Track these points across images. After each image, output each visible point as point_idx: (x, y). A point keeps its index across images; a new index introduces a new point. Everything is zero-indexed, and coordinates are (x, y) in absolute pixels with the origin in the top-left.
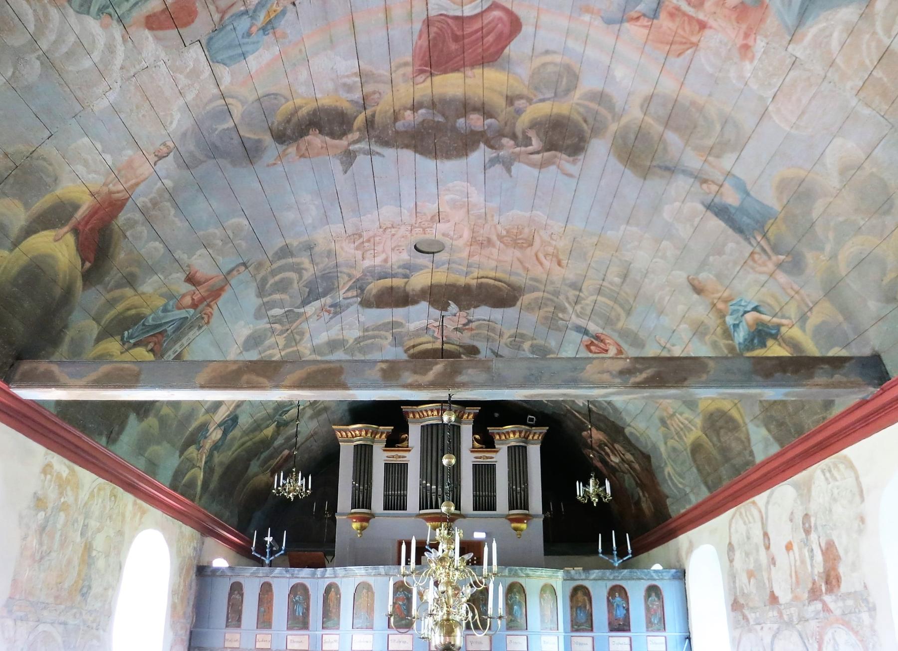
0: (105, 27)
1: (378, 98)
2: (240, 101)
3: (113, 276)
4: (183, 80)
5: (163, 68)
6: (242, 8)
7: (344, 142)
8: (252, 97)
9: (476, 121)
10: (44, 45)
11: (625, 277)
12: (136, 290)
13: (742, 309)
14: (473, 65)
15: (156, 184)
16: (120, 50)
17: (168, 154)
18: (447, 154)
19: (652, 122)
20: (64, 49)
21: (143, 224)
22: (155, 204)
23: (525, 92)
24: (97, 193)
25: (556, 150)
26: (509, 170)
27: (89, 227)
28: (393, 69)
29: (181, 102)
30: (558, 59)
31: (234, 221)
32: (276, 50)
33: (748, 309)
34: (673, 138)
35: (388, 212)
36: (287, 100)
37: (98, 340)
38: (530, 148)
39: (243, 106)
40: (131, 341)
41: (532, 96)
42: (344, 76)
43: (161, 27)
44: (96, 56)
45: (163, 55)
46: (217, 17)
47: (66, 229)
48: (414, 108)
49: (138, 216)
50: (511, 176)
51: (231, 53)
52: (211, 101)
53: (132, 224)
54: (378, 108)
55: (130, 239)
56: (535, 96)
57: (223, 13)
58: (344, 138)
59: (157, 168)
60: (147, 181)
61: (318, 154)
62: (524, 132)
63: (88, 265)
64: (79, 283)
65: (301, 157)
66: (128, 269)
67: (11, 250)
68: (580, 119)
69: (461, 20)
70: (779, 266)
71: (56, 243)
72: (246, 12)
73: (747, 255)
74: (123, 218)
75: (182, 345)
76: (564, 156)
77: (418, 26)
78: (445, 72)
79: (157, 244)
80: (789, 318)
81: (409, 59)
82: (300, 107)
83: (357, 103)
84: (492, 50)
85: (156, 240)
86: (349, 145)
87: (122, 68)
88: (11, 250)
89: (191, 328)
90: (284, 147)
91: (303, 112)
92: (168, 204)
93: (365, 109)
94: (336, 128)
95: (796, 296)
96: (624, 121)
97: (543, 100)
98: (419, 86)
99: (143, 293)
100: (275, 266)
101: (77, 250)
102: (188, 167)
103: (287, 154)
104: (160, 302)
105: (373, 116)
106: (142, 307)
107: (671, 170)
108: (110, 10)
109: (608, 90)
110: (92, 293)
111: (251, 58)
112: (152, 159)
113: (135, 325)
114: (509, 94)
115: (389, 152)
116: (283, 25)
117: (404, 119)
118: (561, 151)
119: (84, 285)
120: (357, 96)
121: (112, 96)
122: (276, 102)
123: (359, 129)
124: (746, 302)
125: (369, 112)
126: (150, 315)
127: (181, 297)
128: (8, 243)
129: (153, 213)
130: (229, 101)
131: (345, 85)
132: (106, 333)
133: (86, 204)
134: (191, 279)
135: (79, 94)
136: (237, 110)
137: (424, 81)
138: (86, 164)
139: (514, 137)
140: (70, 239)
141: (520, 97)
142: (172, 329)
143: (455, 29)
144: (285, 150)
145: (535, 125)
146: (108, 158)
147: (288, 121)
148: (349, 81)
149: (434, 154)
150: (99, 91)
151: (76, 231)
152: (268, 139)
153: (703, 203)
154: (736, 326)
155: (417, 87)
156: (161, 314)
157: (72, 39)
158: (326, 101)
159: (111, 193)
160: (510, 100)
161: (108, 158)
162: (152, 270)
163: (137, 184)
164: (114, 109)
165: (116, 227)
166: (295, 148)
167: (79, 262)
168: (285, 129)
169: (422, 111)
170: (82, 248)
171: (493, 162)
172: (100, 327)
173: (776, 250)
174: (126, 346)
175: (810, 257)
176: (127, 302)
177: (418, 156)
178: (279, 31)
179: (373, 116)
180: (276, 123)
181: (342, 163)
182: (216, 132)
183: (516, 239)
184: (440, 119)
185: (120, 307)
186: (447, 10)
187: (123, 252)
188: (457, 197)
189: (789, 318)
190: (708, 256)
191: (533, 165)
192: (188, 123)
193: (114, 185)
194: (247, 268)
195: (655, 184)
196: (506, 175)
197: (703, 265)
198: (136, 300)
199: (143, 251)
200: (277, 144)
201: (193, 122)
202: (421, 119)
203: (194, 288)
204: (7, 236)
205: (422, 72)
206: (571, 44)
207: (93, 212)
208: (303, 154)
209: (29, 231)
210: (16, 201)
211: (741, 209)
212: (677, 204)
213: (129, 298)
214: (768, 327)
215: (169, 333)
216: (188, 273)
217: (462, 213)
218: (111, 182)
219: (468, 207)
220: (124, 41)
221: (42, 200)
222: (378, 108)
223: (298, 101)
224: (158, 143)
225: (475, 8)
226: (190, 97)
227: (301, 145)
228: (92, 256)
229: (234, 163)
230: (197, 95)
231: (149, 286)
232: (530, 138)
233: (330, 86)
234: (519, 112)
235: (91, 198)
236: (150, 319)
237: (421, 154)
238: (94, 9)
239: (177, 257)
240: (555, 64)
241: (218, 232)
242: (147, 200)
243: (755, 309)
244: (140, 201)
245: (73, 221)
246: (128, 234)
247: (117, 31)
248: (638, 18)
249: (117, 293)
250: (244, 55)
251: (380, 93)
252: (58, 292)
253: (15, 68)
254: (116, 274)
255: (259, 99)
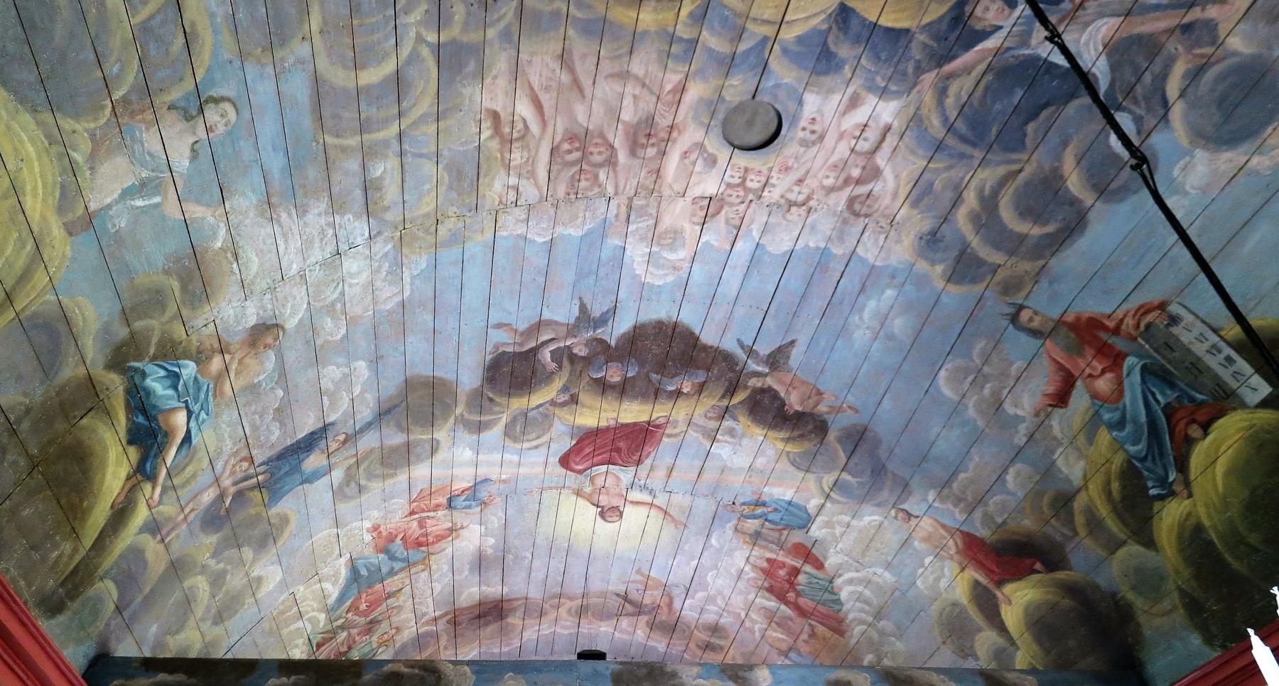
0: (840, 589)
1: (709, 412)
2: (821, 482)
3: (1056, 530)
4: (838, 530)
5: (840, 546)
6: (767, 523)
7: (769, 381)
8: (810, 476)
9: (614, 374)
10: (870, 619)
11: (369, 188)
12: (1078, 491)
13: (196, 408)
14: (608, 429)
15: (937, 509)
16: (847, 576)
17: (903, 510)
18: (661, 329)
19: (423, 437)
20: (867, 608)
21: (986, 505)
22: (959, 500)
23: (557, 411)
24: (961, 564)
25: (521, 353)
26: (583, 308)
27: (996, 570)
28: (683, 434)
29: (854, 523)
30: (526, 445)
31: (947, 391)
32: (766, 489)
33: (193, 424)
34: (397, 439)
35: (780, 243)
36: (788, 453)
37: (1150, 543)
38: (553, 347)
39: (823, 477)
40: (1171, 479)
41: (551, 408)
42: (729, 443)
43: (817, 560)
44: (860, 589)
45: (832, 550)
46: (785, 532)
47: (998, 594)
48: (678, 394)
49: (978, 514)
50: (580, 299)
51: (796, 511)
52: (839, 502)
53: (987, 518)
54: (714, 402)
55: (1005, 516)
56: (547, 409)
57: (780, 530)
58: (766, 386)
59: (920, 514)
60: (938, 518)
61: (804, 383)
62: (560, 367)
63: (1038, 566)
64: (1061, 575)
65: (822, 394)
66: (1045, 509)
67: (1018, 648)
68: (498, 399)
69: (610, 462)
70: (222, 496)
71: (1013, 603)
72: (766, 520)
73: (254, 452)
74: (983, 532)
75: (1214, 349)
76: (510, 349)
77: (648, 462)
78: (635, 424)
79: (1009, 478)
80: (160, 503)
81: (665, 439)
82: (782, 440)
83: (731, 417)
84: (587, 442)
85: (1005, 481)
86: (766, 375)
87: (858, 571)
88: (1018, 648)
89: (1170, 345)
90: (826, 416)
91: (783, 434)
92: (955, 485)
93: (727, 407)
94: (766, 401)
95: (182, 516)
96: (452, 420)
97: (541, 405)
98: (665, 414)
99: (1085, 476)
100: (996, 257)
101: (1020, 579)
102: (907, 485)
103: (830, 407)
104: (1104, 437)
105: (723, 397)
106: (1108, 474)
107: (384, 414)
108: (829, 589)
109: (475, 437)
110: (1076, 558)
111: (788, 498)
112: (914, 522)
113: (1140, 473)
114: (574, 406)
115: (729, 345)
116: (749, 497)
117: (693, 384)
118: (515, 354)
119: (1063, 569)
120: (727, 423)
121: (879, 571)
122: (797, 459)
123: (746, 387)
124: (204, 421)
125: (725, 403)
126: (1126, 451)
127: (1098, 399)
128: (1012, 649)
129: (970, 498)
130: (827, 490)
131: (733, 436)
132: (1143, 533)
133: (973, 574)
134: (1061, 398)
135: (889, 593)
136: (829, 479)
137: (657, 419)
138: (938, 579)
139: (573, 358)
140: (1009, 588)
141: (563, 404)
142: (1163, 393)
143: (617, 457)
144: (828, 413)
145: (549, 377)
146: (928, 560)
147: (802, 436)
148: (727, 438)
149: (677, 330)
150: (880, 580)
151: (1000, 584)
152: (832, 436)
153: (332, 424)
154: (174, 377)
155: (667, 414)
156: (1129, 428)
157: (858, 604)
158: (758, 432)
159: (958, 552)
160: (574, 400)
161: (928, 560)
162: (1049, 471)
163: (944, 526)
164: (888, 566)
165: (994, 537)
166: (819, 407)
167: (1035, 577)
168: (811, 432)
169: (671, 388)
170: (1018, 574)
171: (602, 321)
172: (1129, 541)
173: (239, 495)
174: (1178, 488)
175: (212, 539)
176: (1098, 503)
177: (697, 332)
178: (755, 498)
179: (723, 397)
180: (813, 443)
181: (788, 357)
182: (860, 480)
183: (581, 160)
184: (654, 377)
185: (1103, 511)
186: (621, 470)
187: (1022, 523)
188: (665, 256)
189: (160, 503)
190: (286, 391)
191: (550, 323)
192: (867, 508)
193: (950, 549)
194: (1021, 308)
195: (391, 384)
196: (587, 301)
197: (282, 375)
198: (1094, 489)
199: (1021, 494)
200: (830, 424)
201: (863, 506)
202: (676, 379)
203: (1079, 383)
204: (1005, 649)
205: (658, 427)
206: (516, 458)
207: (981, 565)
208: (816, 395)
209: (1002, 628)
210: (977, 638)
211: (296, 469)
212: (357, 390)
213: (1094, 498)
214: (156, 456)
215: (1172, 395)
216: (1050, 409)
217: (667, 222)
218: (948, 553)
219: (655, 236)
220: (840, 576)
221: (974, 617)
222: (714, 402)
223: (780, 445)
224: (899, 523)
225: (596, 470)
226: (846, 518)
227: (811, 406)
228: (1028, 561)
229: (877, 443)
230: (841, 514)
231: (1072, 468)
232: (552, 361)
233: (745, 441)
234: (565, 389)
235: (967, 571)
236: (1132, 449)
237: (692, 334)
238: (835, 597)
239: (1025, 439)
240: (528, 440)
241: (971, 402)
242: (957, 510)
243: (188, 438)
244: (960, 516)
245: (991, 586)
246: (1000, 520)
247: (838, 582)
248: (463, 492)
249: (1079, 520)
250: (790, 503)
251: (706, 416)
252: (1067, 603)
253: (889, 635)
254: (1053, 527)
255: (807, 471)
